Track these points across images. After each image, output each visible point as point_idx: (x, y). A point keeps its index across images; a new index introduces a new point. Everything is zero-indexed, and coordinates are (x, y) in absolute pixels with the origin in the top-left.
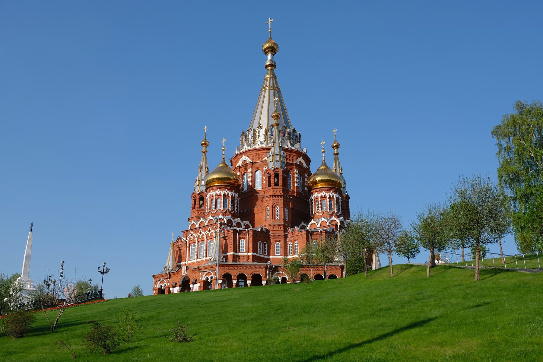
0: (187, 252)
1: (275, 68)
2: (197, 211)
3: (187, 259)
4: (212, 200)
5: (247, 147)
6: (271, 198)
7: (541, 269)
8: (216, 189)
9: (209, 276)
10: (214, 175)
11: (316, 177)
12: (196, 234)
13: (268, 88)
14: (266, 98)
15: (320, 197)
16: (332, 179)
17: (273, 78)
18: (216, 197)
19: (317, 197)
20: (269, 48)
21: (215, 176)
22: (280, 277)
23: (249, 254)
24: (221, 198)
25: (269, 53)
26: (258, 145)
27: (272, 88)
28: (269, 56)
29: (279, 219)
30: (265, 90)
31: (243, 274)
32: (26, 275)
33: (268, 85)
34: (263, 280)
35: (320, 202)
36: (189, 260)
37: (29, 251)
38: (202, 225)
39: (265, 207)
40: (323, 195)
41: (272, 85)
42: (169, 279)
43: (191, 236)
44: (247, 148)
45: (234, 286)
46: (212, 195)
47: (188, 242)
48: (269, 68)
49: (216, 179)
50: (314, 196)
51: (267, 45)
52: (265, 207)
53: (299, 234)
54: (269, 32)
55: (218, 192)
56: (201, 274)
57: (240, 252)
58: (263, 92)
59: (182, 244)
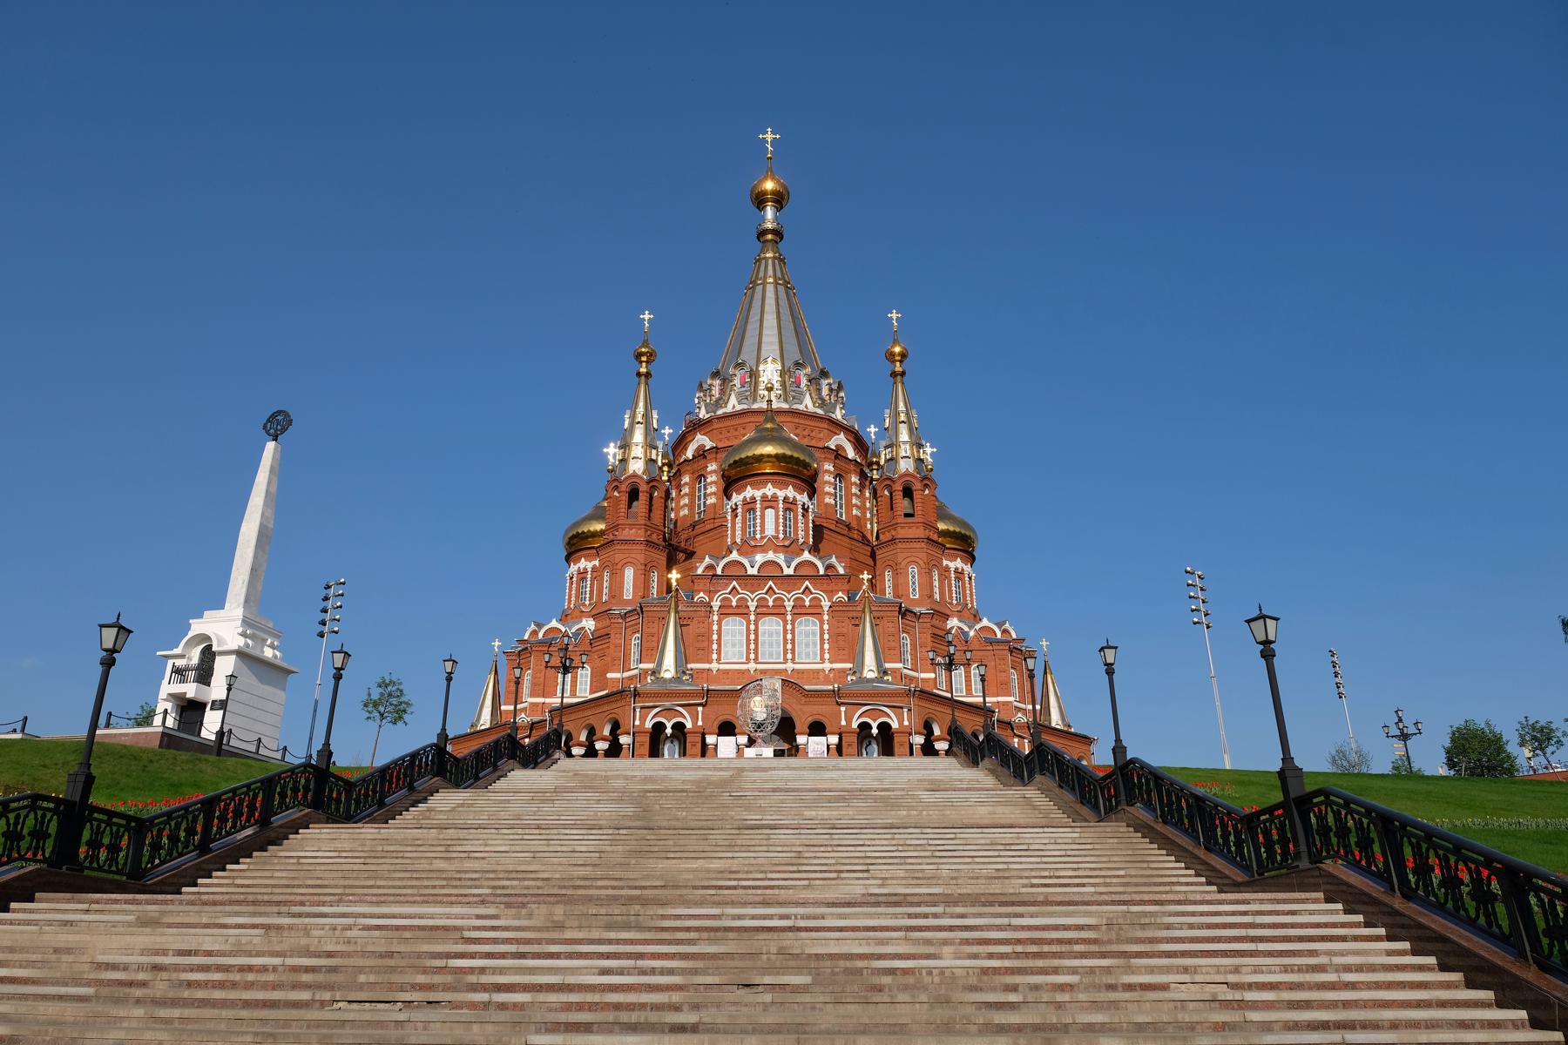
0: (715, 637)
1: (782, 238)
2: (645, 525)
3: (715, 656)
5: (736, 404)
6: (923, 545)
7: (2, 772)
8: (764, 484)
9: (874, 720)
12: (752, 592)
13: (771, 280)
15: (781, 498)
16: (963, 532)
19: (585, 569)
21: (769, 449)
24: (797, 512)
25: (770, 204)
26: (734, 407)
28: (769, 212)
29: (917, 596)
30: (764, 284)
31: (724, 723)
33: (770, 272)
34: (575, 745)
35: (589, 582)
36: (718, 660)
38: (732, 568)
39: (621, 564)
40: (769, 494)
41: (779, 274)
42: (700, 709)
44: (739, 407)
48: (770, 237)
52: (621, 564)
55: (769, 490)
56: (843, 709)
57: (760, 660)
58: (759, 288)
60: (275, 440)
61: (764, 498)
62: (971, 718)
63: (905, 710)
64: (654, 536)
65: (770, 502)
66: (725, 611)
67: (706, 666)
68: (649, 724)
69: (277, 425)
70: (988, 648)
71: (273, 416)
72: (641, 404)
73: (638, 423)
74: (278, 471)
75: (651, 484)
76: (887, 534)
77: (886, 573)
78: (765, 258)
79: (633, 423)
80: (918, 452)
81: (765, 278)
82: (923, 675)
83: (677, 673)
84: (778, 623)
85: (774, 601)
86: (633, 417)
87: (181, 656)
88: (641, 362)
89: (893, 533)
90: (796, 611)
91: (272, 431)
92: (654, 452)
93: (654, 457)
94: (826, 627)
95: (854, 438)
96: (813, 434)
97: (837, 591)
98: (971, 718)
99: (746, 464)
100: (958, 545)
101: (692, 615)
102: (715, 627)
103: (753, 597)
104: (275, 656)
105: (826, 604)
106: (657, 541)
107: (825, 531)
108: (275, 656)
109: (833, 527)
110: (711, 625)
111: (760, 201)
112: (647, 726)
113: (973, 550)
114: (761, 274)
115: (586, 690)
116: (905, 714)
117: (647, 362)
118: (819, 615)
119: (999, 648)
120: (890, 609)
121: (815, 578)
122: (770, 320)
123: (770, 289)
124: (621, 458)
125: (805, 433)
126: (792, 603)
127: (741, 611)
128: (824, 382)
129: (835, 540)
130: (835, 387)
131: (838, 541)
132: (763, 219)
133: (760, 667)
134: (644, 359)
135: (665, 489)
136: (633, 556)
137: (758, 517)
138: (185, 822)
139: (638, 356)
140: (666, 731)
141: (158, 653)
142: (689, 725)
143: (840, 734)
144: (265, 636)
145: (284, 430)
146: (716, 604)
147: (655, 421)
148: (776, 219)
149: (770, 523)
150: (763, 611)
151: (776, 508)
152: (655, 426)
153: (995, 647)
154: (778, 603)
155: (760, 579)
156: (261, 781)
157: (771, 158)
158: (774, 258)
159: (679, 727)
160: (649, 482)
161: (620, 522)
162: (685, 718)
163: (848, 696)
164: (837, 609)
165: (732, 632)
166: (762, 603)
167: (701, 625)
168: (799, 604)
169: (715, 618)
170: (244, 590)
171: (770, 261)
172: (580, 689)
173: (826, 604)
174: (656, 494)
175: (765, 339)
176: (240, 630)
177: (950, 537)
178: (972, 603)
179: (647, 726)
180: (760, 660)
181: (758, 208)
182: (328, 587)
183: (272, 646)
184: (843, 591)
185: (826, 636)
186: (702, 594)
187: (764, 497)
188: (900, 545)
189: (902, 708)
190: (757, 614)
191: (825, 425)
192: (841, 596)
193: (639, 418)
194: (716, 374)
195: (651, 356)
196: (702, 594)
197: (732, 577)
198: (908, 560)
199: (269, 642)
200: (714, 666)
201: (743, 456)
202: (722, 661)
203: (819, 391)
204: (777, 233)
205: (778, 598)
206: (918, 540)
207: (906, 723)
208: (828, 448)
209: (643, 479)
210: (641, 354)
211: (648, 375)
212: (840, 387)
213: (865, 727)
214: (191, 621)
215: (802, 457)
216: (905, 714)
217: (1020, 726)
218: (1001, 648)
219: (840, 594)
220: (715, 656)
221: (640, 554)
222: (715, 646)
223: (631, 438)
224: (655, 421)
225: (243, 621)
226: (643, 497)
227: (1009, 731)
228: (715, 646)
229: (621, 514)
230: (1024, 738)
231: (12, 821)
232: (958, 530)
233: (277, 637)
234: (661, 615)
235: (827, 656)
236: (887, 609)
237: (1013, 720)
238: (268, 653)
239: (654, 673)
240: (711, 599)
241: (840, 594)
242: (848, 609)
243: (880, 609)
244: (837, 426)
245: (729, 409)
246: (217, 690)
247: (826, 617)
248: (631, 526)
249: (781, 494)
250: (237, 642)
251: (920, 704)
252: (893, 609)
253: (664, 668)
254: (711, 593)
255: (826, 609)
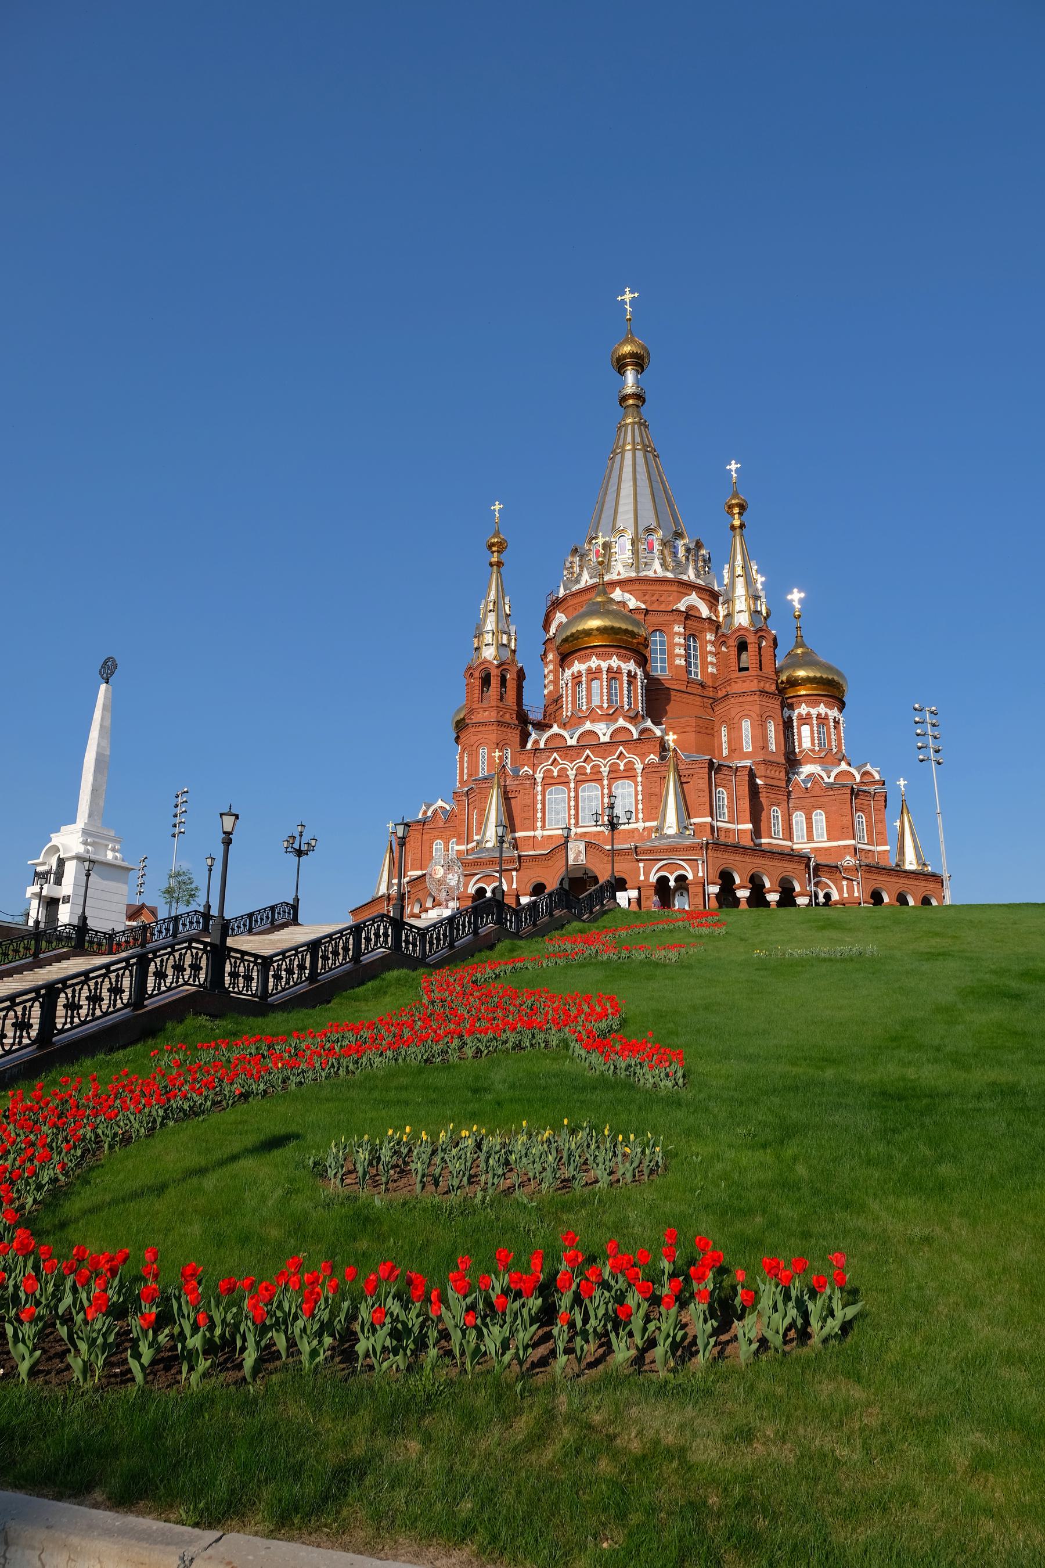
0: (539, 806)
1: (644, 401)
3: (539, 824)
4: (579, 683)
5: (588, 579)
6: (756, 698)
8: (588, 658)
9: (671, 874)
10: (591, 619)
11: (794, 671)
12: (604, 759)
14: (628, 469)
15: (605, 669)
16: (825, 676)
17: (640, 424)
18: (587, 677)
19: (579, 672)
20: (632, 355)
21: (594, 623)
22: (822, 890)
23: (741, 827)
25: (629, 368)
26: (619, 574)
27: (639, 447)
28: (630, 376)
32: (96, 818)
33: (629, 439)
35: (584, 686)
36: (543, 827)
37: (105, 743)
38: (556, 741)
41: (638, 439)
42: (514, 873)
43: (618, 758)
44: (591, 582)
45: (743, 905)
46: (579, 672)
47: (539, 780)
48: (631, 402)
49: (598, 629)
50: (796, 712)
51: (627, 349)
53: (826, 794)
54: (627, 320)
55: (594, 663)
56: (641, 865)
57: (580, 825)
58: (618, 457)
59: (518, 782)
60: (107, 683)
61: (589, 670)
62: (780, 865)
63: (700, 862)
64: (507, 716)
65: (594, 674)
66: (549, 781)
67: (531, 833)
68: (653, 879)
69: (108, 670)
70: (829, 793)
71: (105, 662)
72: (739, 557)
73: (490, 611)
74: (114, 707)
75: (502, 668)
76: (724, 690)
77: (723, 729)
78: (626, 425)
79: (733, 576)
80: (755, 604)
81: (624, 444)
82: (741, 827)
83: (679, 829)
84: (630, 785)
85: (592, 768)
86: (732, 570)
87: (43, 864)
88: (493, 552)
89: (728, 688)
90: (612, 776)
91: (105, 675)
92: (505, 637)
93: (505, 641)
94: (640, 788)
95: (709, 596)
96: (661, 599)
97: (649, 754)
98: (780, 865)
99: (577, 638)
100: (823, 691)
101: (519, 788)
102: (539, 797)
103: (571, 766)
104: (116, 858)
105: (639, 766)
106: (510, 721)
107: (673, 693)
108: (116, 858)
109: (683, 688)
110: (534, 796)
111: (620, 366)
112: (651, 880)
113: (843, 696)
114: (621, 443)
115: (822, 835)
116: (700, 866)
117: (739, 513)
118: (633, 777)
119: (840, 792)
120: (700, 766)
121: (629, 743)
122: (627, 488)
123: (628, 456)
124: (725, 613)
125: (655, 598)
126: (607, 769)
127: (562, 780)
128: (680, 543)
129: (684, 700)
130: (692, 546)
131: (689, 701)
132: (624, 383)
133: (546, 833)
134: (495, 549)
135: (516, 670)
136: (486, 736)
137: (584, 689)
138: (295, 980)
139: (731, 507)
140: (670, 884)
141: (29, 863)
142: (690, 877)
143: (639, 889)
144: (106, 842)
145: (112, 673)
146: (539, 776)
147: (507, 607)
148: (637, 382)
149: (598, 694)
150: (582, 779)
151: (600, 679)
152: (508, 612)
153: (836, 792)
154: (595, 770)
155: (579, 748)
156: (307, 944)
157: (630, 319)
158: (634, 423)
159: (681, 879)
160: (499, 666)
161: (732, 676)
162: (686, 870)
163: (645, 852)
164: (650, 770)
165: (557, 800)
166: (580, 771)
167: (527, 797)
168: (614, 769)
169: (539, 788)
170: (88, 807)
171: (630, 427)
172: (818, 835)
173: (639, 766)
174: (764, 643)
175: (621, 509)
176: (81, 840)
177: (817, 683)
178: (839, 746)
179: (651, 880)
180: (580, 825)
181: (619, 372)
182: (177, 797)
183: (113, 850)
184: (654, 753)
185: (640, 797)
186: (526, 768)
187: (589, 669)
188: (733, 700)
189: (696, 860)
190: (610, 779)
191: (674, 588)
192: (653, 757)
193: (739, 571)
194: (575, 551)
195: (501, 547)
196: (526, 768)
197: (621, 743)
198: (740, 714)
199: (110, 847)
200: (539, 833)
201: (574, 630)
202: (547, 827)
203: (675, 554)
204: (639, 397)
205: (629, 762)
206: (751, 693)
207: (700, 874)
208: (678, 611)
209: (493, 663)
210: (493, 545)
211: (499, 564)
212: (699, 545)
213: (663, 881)
214: (51, 835)
215: (630, 628)
216: (700, 866)
217: (848, 869)
218: (842, 792)
219: (652, 756)
220: (539, 824)
221: (755, 705)
222: (539, 815)
223: (733, 591)
224: (507, 607)
225: (83, 832)
226: (752, 648)
227: (838, 874)
228: (539, 815)
229: (476, 699)
230: (852, 880)
231: (92, 988)
232: (818, 675)
233: (119, 842)
234: (662, 775)
235: (641, 816)
236: (697, 766)
237: (839, 863)
238: (110, 855)
239: (657, 829)
240: (534, 772)
241: (652, 756)
242: (659, 769)
243: (690, 766)
244: (691, 587)
245: (582, 585)
246: (67, 887)
247: (639, 779)
248: (485, 709)
249: (604, 665)
250: (80, 849)
251: (715, 855)
252: (703, 765)
253: (667, 824)
254: (534, 767)
255: (639, 771)
